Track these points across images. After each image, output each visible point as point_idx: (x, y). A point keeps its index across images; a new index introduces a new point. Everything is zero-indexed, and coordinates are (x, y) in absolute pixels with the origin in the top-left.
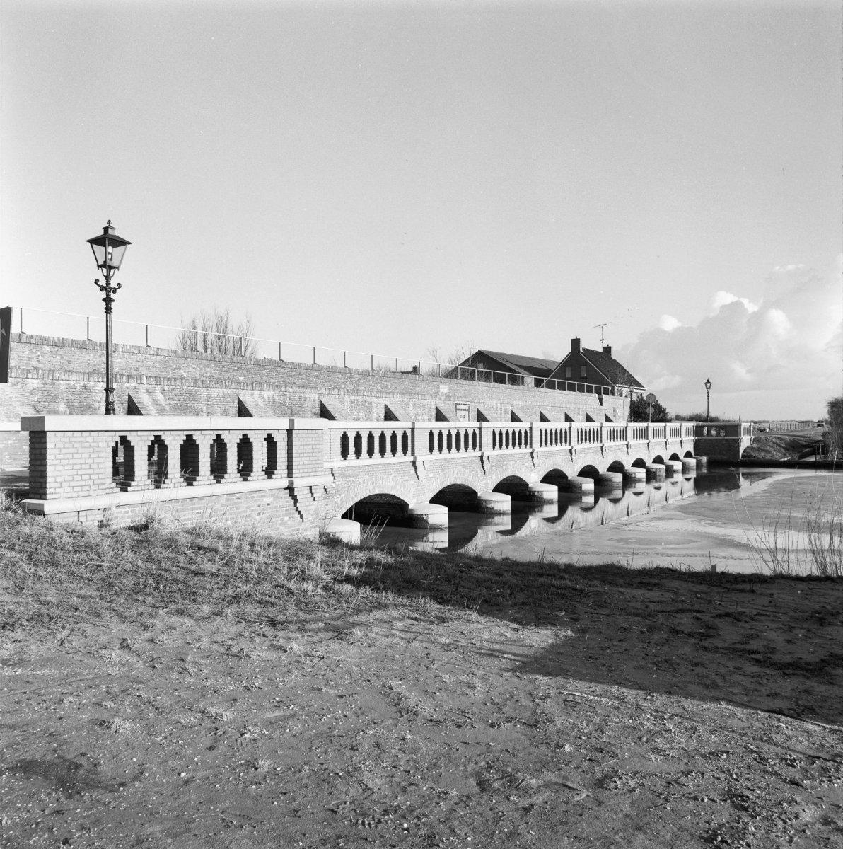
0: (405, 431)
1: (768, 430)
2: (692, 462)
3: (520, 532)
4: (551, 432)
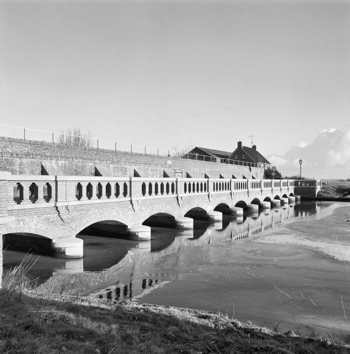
0: (173, 183)
1: (326, 183)
2: (293, 198)
3: (203, 236)
4: (220, 184)
